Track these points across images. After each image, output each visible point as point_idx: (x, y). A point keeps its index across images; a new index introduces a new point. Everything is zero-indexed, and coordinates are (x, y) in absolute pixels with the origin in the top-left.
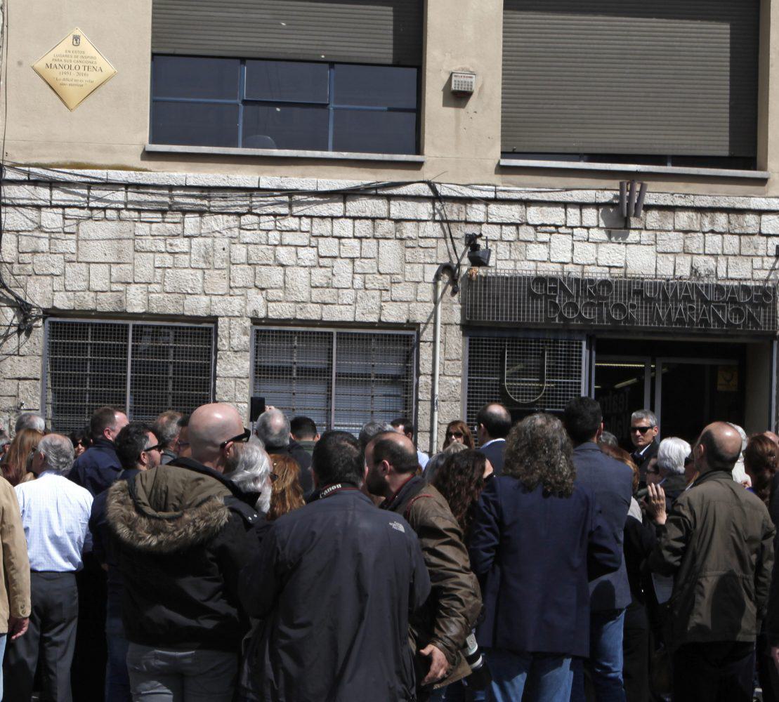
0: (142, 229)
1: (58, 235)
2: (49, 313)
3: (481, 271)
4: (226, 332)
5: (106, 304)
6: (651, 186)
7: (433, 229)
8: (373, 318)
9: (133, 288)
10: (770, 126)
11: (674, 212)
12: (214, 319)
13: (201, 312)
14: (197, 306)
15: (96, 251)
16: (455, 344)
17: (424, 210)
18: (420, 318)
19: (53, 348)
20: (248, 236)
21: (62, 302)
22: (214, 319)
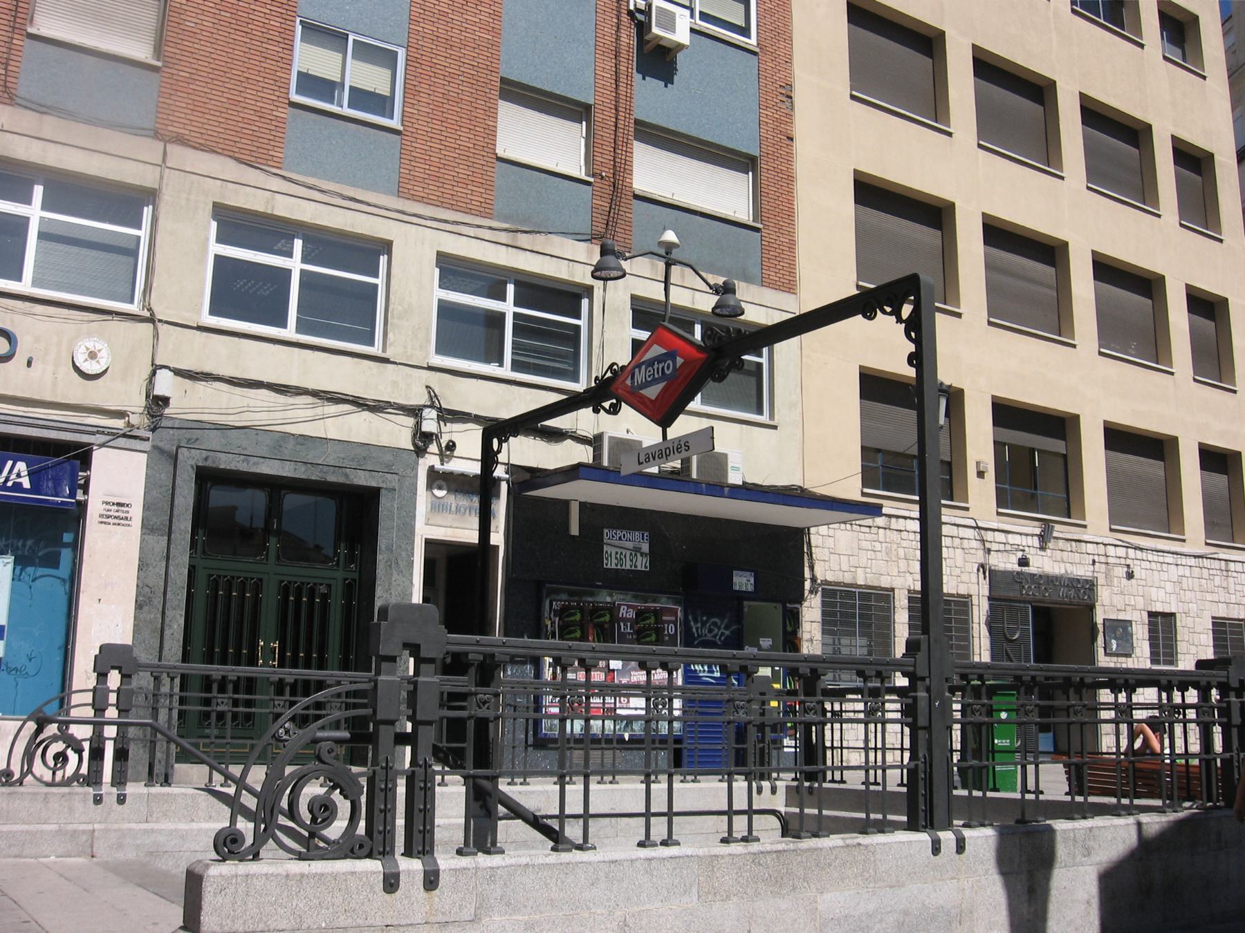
0: (862, 536)
1: (1118, 561)
2: (826, 582)
3: (1025, 569)
4: (165, 689)
5: (848, 579)
6: (1057, 527)
7: (975, 544)
8: (954, 592)
9: (859, 570)
10: (924, 228)
11: (744, 483)
12: (893, 590)
13: (888, 586)
14: (885, 582)
15: (842, 547)
16: (985, 605)
17: (970, 533)
18: (972, 593)
19: (824, 604)
20: (904, 544)
21: (830, 578)
22: (893, 590)
